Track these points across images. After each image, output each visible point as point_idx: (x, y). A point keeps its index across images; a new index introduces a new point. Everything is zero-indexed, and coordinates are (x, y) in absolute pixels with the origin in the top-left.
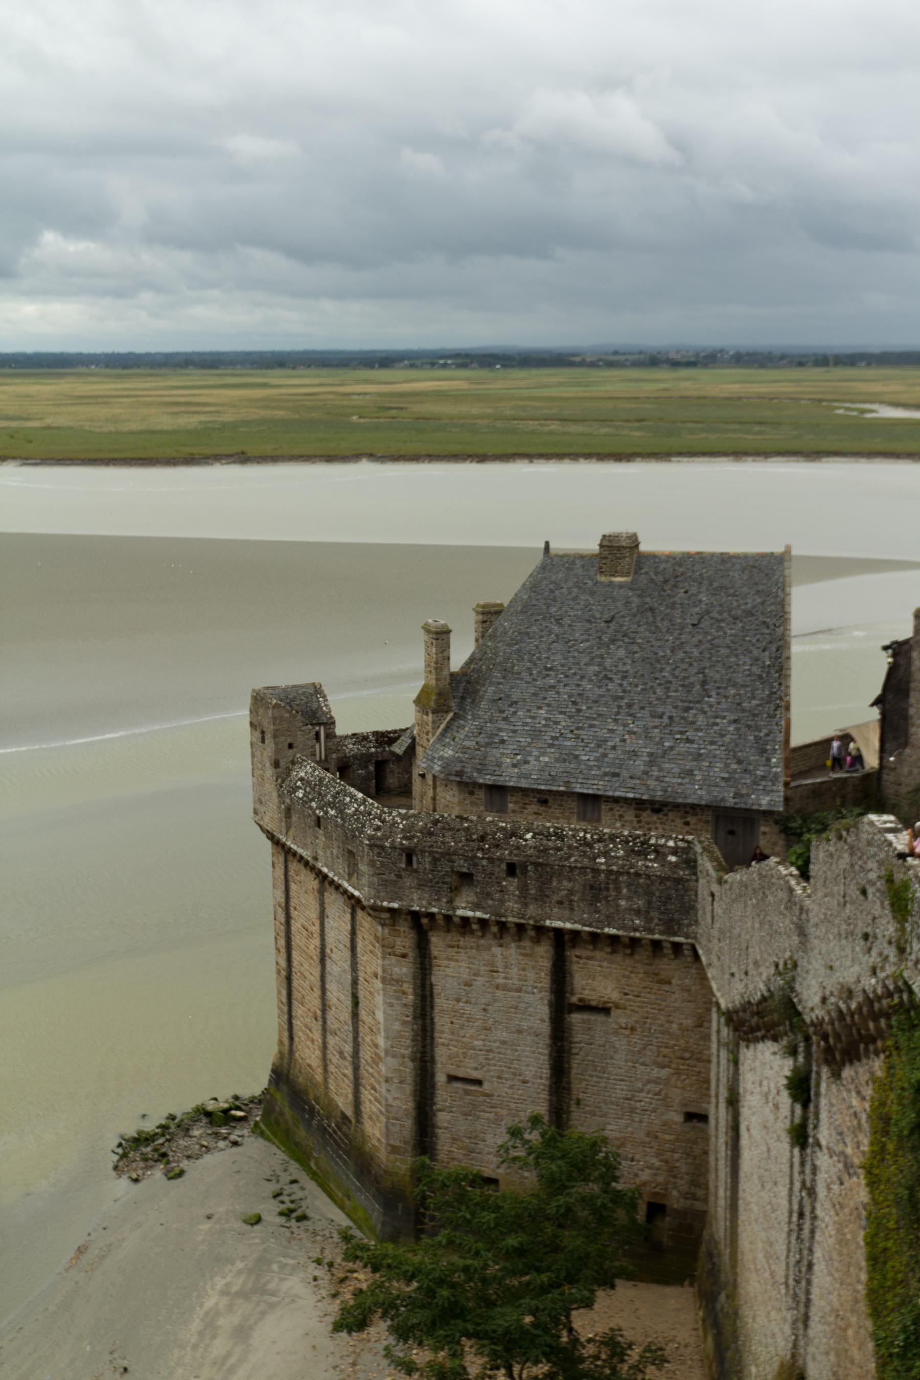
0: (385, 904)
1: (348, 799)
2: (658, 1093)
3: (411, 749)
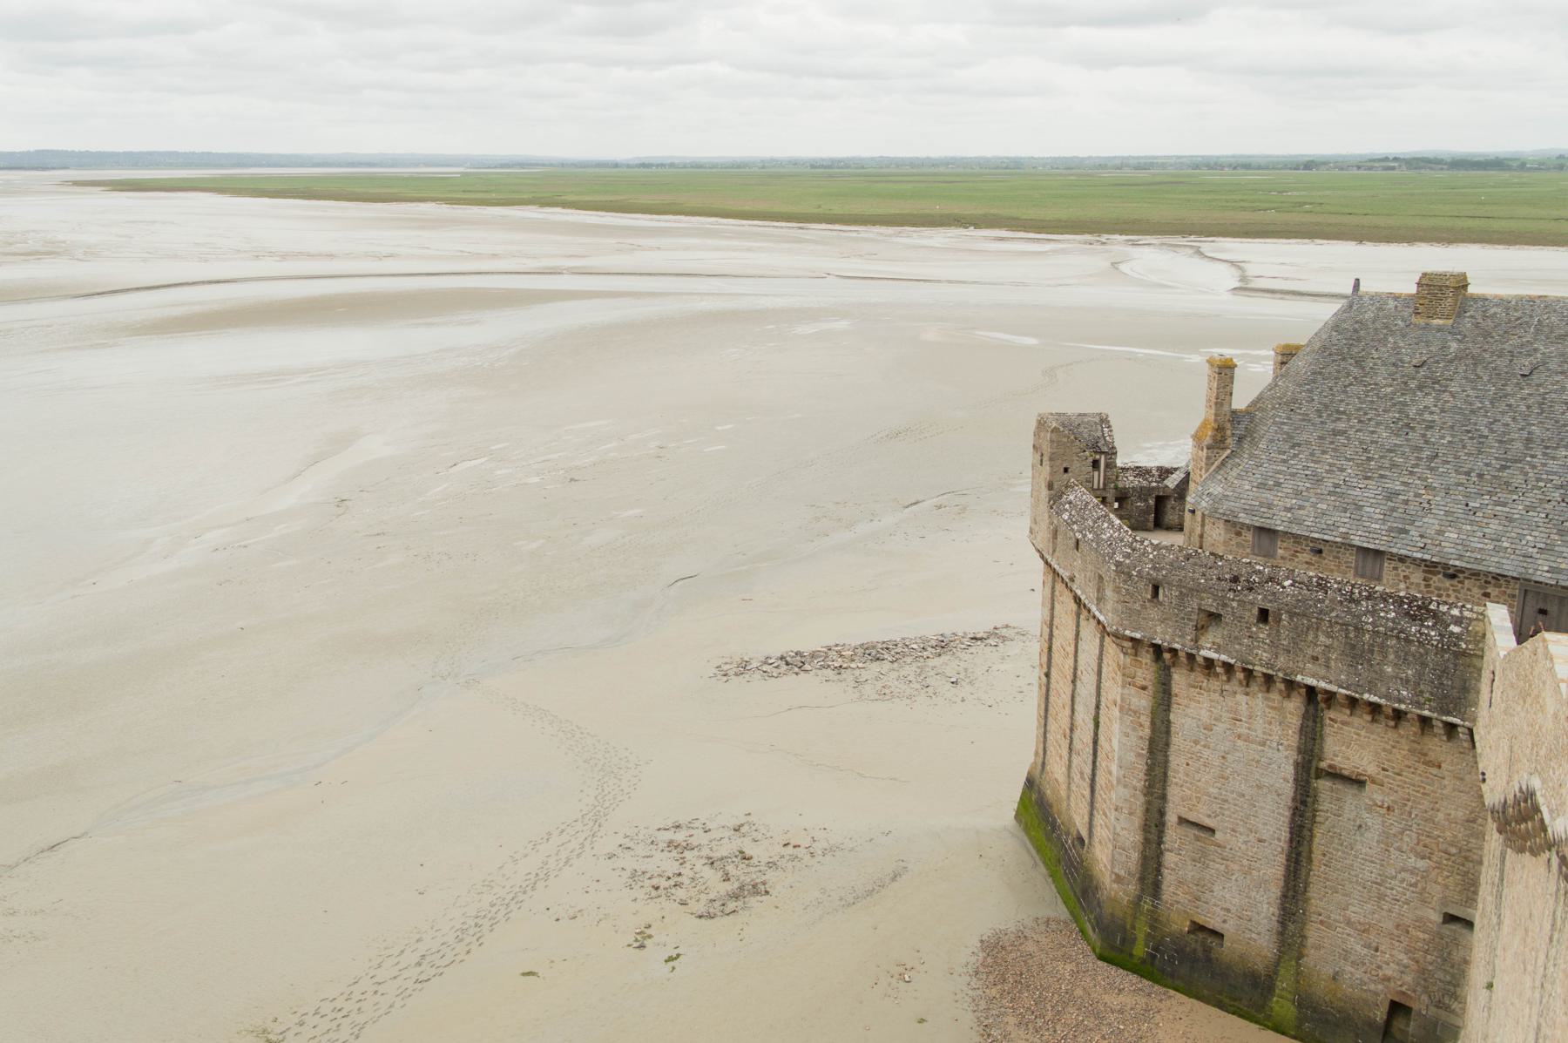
0: (1127, 632)
2: (1415, 885)
3: (1185, 481)
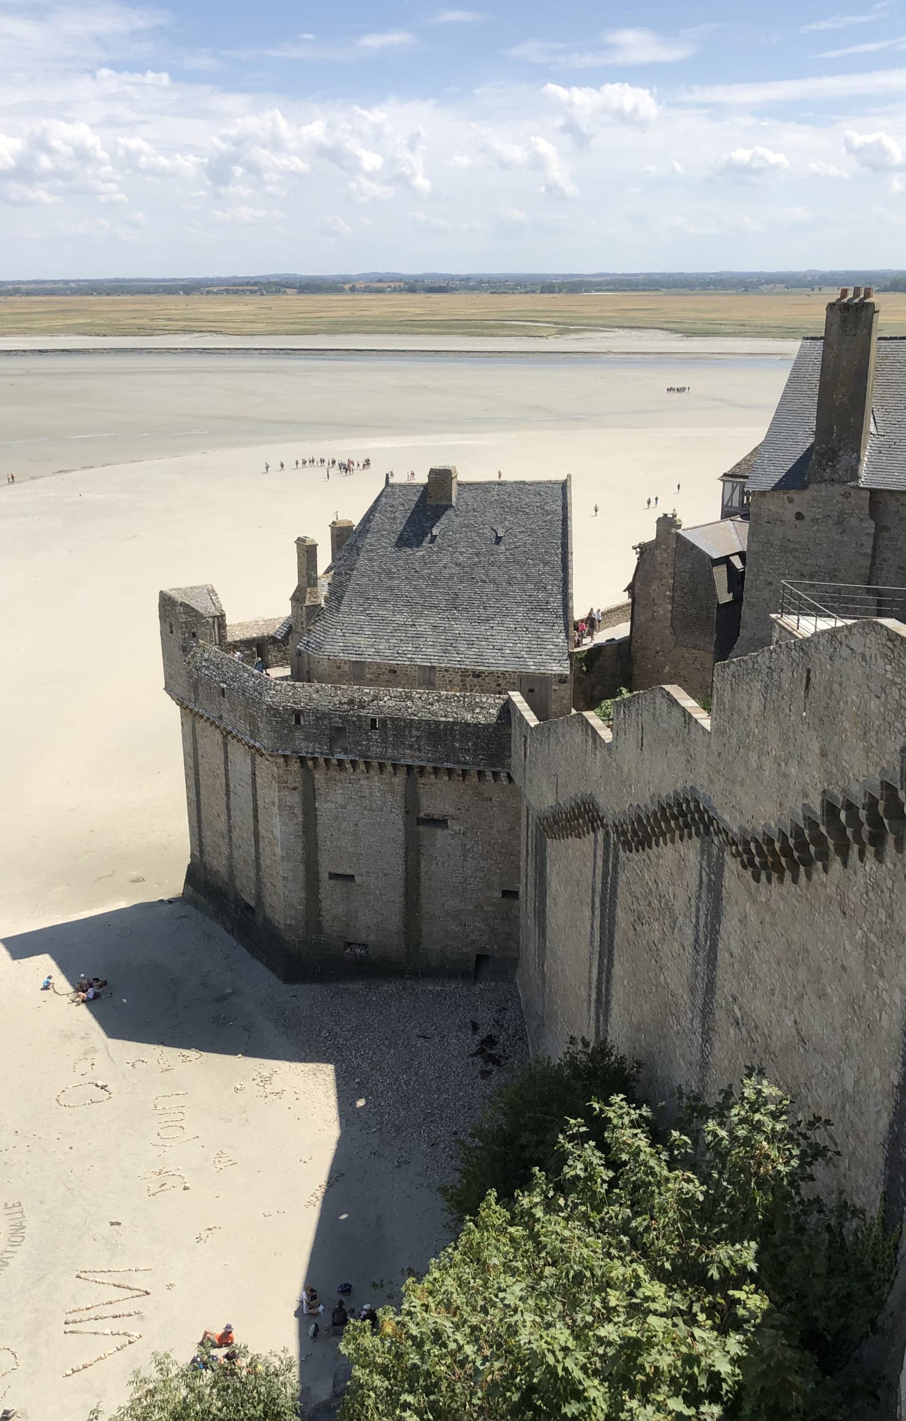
1: (246, 675)
